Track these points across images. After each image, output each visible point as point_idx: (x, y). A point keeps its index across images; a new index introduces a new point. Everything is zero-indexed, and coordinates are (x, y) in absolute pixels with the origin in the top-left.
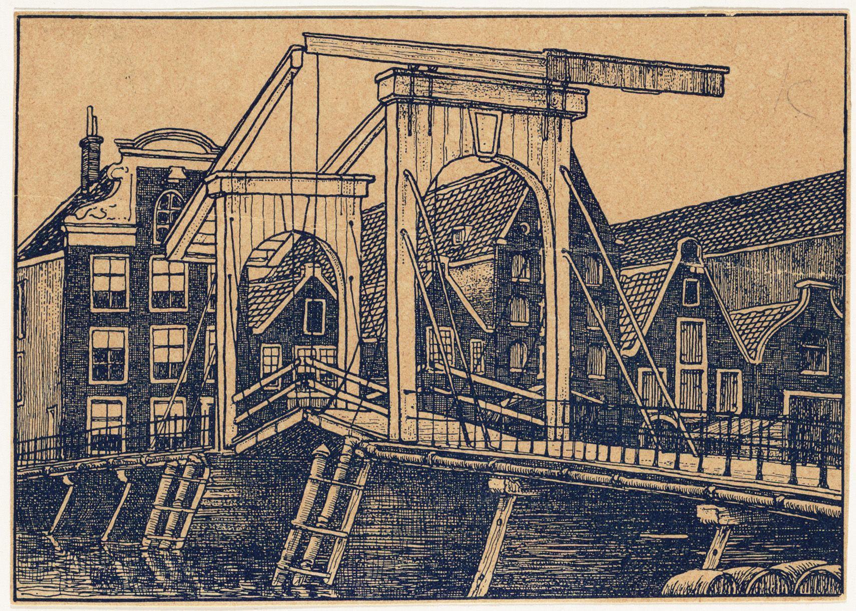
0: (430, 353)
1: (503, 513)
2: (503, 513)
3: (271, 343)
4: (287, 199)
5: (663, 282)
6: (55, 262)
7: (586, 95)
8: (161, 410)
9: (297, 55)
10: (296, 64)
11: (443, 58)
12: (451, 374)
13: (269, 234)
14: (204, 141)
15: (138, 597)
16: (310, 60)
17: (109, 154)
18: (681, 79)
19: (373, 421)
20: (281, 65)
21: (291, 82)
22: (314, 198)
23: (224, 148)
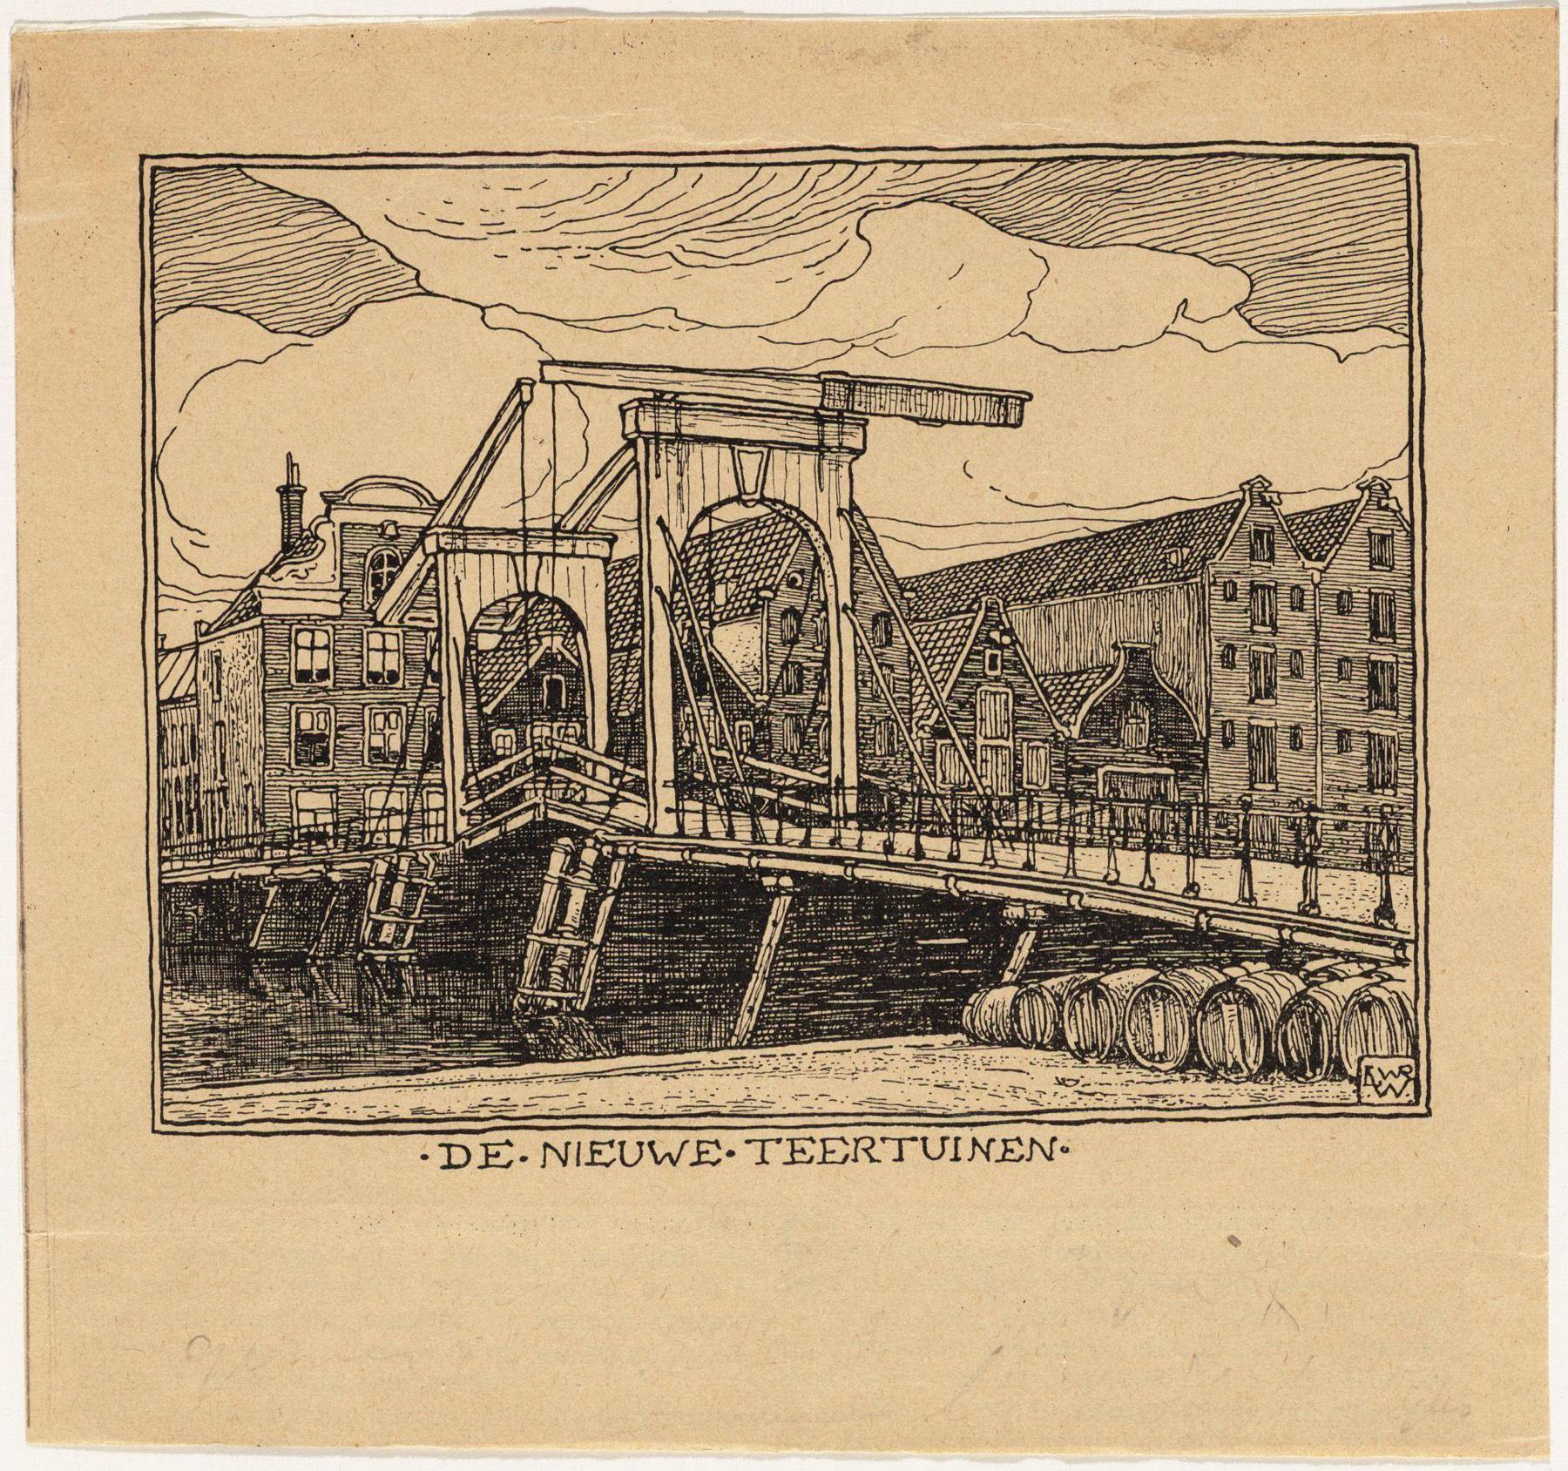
0: (982, 761)
1: (780, 906)
2: (780, 906)
3: (646, 739)
4: (519, 560)
5: (959, 653)
6: (1412, 792)
7: (864, 426)
8: (378, 800)
9: (525, 389)
10: (526, 398)
11: (687, 383)
12: (712, 757)
13: (487, 601)
14: (416, 489)
15: (1144, 893)
16: (542, 391)
17: (313, 506)
18: (971, 408)
19: (631, 811)
20: (509, 400)
21: (522, 418)
22: (550, 558)
23: (641, 554)
